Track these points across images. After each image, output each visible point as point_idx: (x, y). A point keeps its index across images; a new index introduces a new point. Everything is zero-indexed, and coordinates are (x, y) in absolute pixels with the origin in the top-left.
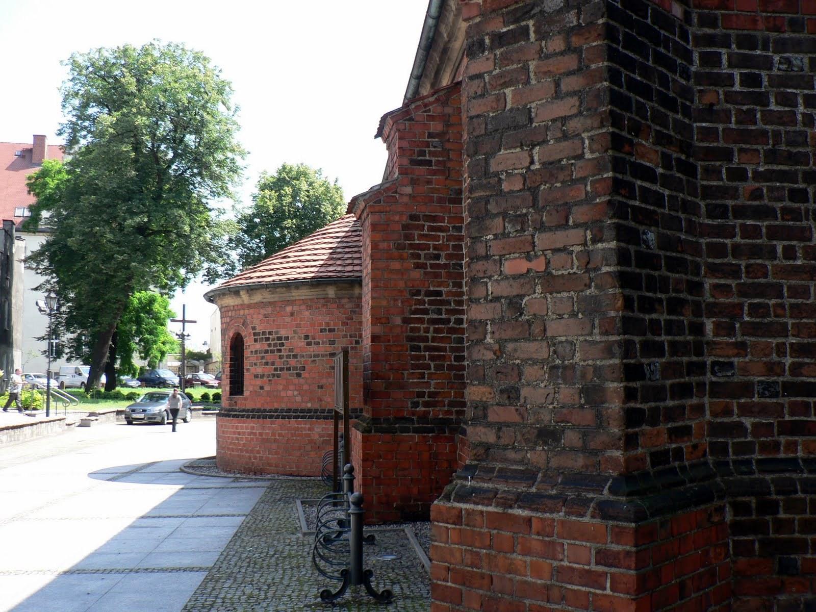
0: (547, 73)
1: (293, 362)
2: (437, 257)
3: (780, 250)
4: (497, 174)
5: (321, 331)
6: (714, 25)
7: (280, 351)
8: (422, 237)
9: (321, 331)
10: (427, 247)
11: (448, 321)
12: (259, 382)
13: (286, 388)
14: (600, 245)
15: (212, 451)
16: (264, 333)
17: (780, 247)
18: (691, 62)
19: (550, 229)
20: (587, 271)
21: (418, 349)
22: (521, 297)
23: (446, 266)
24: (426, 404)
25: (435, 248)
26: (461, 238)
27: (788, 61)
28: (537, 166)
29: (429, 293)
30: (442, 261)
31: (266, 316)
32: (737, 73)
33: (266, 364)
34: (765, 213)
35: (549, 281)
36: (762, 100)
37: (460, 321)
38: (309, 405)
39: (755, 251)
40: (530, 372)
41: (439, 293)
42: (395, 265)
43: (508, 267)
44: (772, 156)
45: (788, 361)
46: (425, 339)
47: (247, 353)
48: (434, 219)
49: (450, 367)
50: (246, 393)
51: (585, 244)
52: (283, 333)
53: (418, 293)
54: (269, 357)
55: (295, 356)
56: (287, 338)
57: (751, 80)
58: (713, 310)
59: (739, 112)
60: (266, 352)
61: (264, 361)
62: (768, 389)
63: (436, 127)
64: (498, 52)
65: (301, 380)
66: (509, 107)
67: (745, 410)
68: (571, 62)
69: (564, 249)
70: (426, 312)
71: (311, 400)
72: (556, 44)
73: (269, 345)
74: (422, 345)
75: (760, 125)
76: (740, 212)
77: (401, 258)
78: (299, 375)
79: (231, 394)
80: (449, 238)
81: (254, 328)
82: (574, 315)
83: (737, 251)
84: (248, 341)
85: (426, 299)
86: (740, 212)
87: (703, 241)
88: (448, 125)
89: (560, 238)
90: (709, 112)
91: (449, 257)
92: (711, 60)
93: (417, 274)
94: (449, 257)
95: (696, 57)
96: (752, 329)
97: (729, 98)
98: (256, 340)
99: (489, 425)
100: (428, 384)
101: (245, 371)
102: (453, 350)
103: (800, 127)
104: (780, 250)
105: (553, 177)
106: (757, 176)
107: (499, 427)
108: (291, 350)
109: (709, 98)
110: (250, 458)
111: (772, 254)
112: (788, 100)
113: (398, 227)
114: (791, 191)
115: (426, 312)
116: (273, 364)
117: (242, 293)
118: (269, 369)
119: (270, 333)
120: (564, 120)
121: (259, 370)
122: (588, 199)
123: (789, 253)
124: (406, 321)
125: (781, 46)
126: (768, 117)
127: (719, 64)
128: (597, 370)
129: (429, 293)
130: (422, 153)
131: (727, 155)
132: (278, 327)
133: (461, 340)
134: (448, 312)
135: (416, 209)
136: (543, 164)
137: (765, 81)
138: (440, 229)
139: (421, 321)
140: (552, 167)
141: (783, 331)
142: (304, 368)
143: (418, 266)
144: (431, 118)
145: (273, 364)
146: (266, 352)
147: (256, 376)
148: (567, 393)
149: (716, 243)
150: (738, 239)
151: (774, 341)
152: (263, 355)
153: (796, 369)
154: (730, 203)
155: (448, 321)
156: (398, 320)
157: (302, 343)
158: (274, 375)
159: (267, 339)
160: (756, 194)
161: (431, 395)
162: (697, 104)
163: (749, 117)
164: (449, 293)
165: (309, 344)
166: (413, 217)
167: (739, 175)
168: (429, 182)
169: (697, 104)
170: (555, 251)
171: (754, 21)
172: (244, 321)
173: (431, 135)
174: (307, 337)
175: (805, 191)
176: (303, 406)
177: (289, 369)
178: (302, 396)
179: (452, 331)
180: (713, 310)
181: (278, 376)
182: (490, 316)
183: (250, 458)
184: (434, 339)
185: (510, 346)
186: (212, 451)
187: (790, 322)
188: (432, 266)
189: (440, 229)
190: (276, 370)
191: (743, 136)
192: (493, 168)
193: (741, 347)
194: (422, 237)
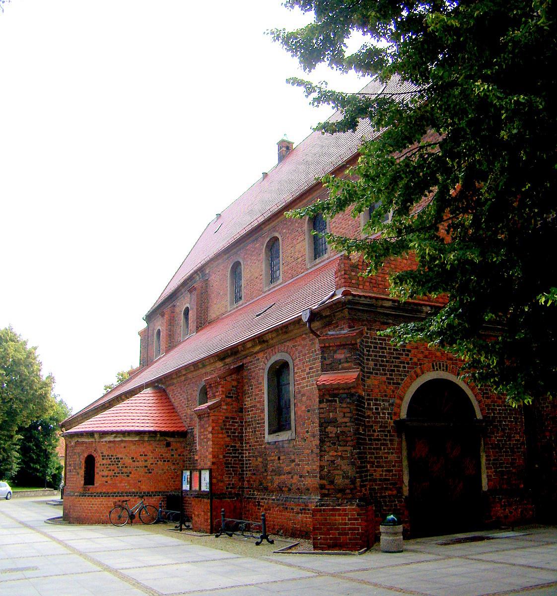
0: (341, 411)
1: (125, 470)
2: (235, 433)
3: (382, 448)
4: (328, 432)
5: (141, 455)
6: (370, 396)
7: (118, 464)
8: (229, 425)
9: (141, 455)
10: (231, 429)
11: (238, 457)
12: (105, 479)
13: (121, 482)
14: (354, 451)
15: (62, 515)
16: (108, 456)
17: (382, 447)
18: (365, 405)
19: (342, 446)
20: (352, 456)
21: (228, 467)
22: (334, 460)
23: (237, 436)
24: (231, 488)
25: (234, 429)
26: (243, 426)
27: (384, 404)
28: (339, 432)
29: (232, 446)
30: (237, 434)
31: (109, 447)
32: (374, 407)
33: (110, 470)
34: (379, 440)
35: (342, 458)
36: (379, 413)
37: (242, 457)
38: (134, 490)
39: (377, 449)
40: (337, 477)
41: (235, 446)
42: (220, 435)
43: (331, 454)
44: (381, 427)
45: (384, 473)
46: (231, 464)
47: (97, 465)
48: (233, 418)
49: (240, 474)
50: (96, 485)
51: (351, 450)
52: (119, 456)
53: (228, 446)
54: (112, 467)
55: (126, 467)
56: (122, 459)
57: (377, 409)
58: (369, 462)
59: (375, 417)
60: (110, 465)
61: (108, 469)
62: (380, 480)
63: (234, 383)
64: (328, 404)
65: (129, 478)
66: (331, 417)
67: (376, 485)
68: (348, 410)
69: (346, 451)
70: (231, 453)
71: (135, 488)
72: (344, 405)
73: (112, 461)
74: (229, 466)
75: (379, 420)
76: (375, 440)
77: (222, 433)
78: (128, 476)
79: (85, 484)
80: (239, 426)
81: (102, 453)
82: (348, 465)
83: (374, 449)
84: (99, 461)
85: (231, 449)
86: (375, 440)
87: (367, 447)
88: (239, 382)
89: (345, 448)
90: (369, 417)
91: (239, 433)
92: (369, 404)
93: (228, 439)
94: (239, 433)
95: (366, 403)
96: (377, 467)
97: (373, 413)
98: (103, 459)
99: (326, 489)
100: (232, 480)
101: (96, 474)
102: (240, 468)
103: (386, 420)
104: (382, 448)
105: (343, 435)
106: (378, 431)
107: (328, 490)
108: (124, 464)
109: (369, 414)
110: (99, 516)
111: (381, 449)
112: (384, 413)
113: (221, 421)
114: (385, 434)
115: (231, 453)
116: (113, 470)
117: (95, 436)
118: (112, 473)
119: (112, 456)
120: (346, 423)
121: (106, 473)
122: (352, 440)
123: (384, 449)
124: (224, 457)
125: (383, 401)
126: (380, 417)
127: (371, 405)
128: (355, 477)
129: (232, 446)
130: (229, 393)
131: (372, 426)
132: (117, 453)
133: (243, 464)
134: (239, 453)
135: (228, 415)
136: (340, 432)
137: (380, 409)
138: (237, 423)
139: (229, 457)
140: (343, 433)
141: (383, 467)
142: (131, 473)
143: (228, 436)
144: (233, 380)
145: (113, 470)
146: (110, 465)
147: (103, 476)
148: (347, 481)
149: (269, 402)
150: (374, 446)
151: (381, 469)
152: (108, 466)
153: (386, 475)
154: (373, 438)
155: (238, 457)
156: (221, 457)
157: (131, 461)
158: (114, 476)
159: (110, 459)
160: (378, 435)
161: (233, 484)
162: (366, 415)
163: (376, 418)
164: (239, 446)
165: (134, 461)
166: (227, 418)
167: (374, 431)
168: (232, 404)
169: (366, 415)
170: (343, 451)
171: (377, 395)
172: (95, 449)
173: (233, 387)
174: (133, 458)
175: (387, 435)
176: (130, 490)
177: (122, 473)
178: (130, 486)
179: (240, 460)
180: (369, 462)
181: (117, 476)
182: (326, 464)
183: (99, 516)
184: (234, 464)
185: (332, 472)
186: (62, 515)
187: (384, 465)
188: (233, 436)
189: (237, 423)
190: (115, 473)
191: (375, 422)
192: (327, 431)
193: (375, 471)
194: (229, 425)
